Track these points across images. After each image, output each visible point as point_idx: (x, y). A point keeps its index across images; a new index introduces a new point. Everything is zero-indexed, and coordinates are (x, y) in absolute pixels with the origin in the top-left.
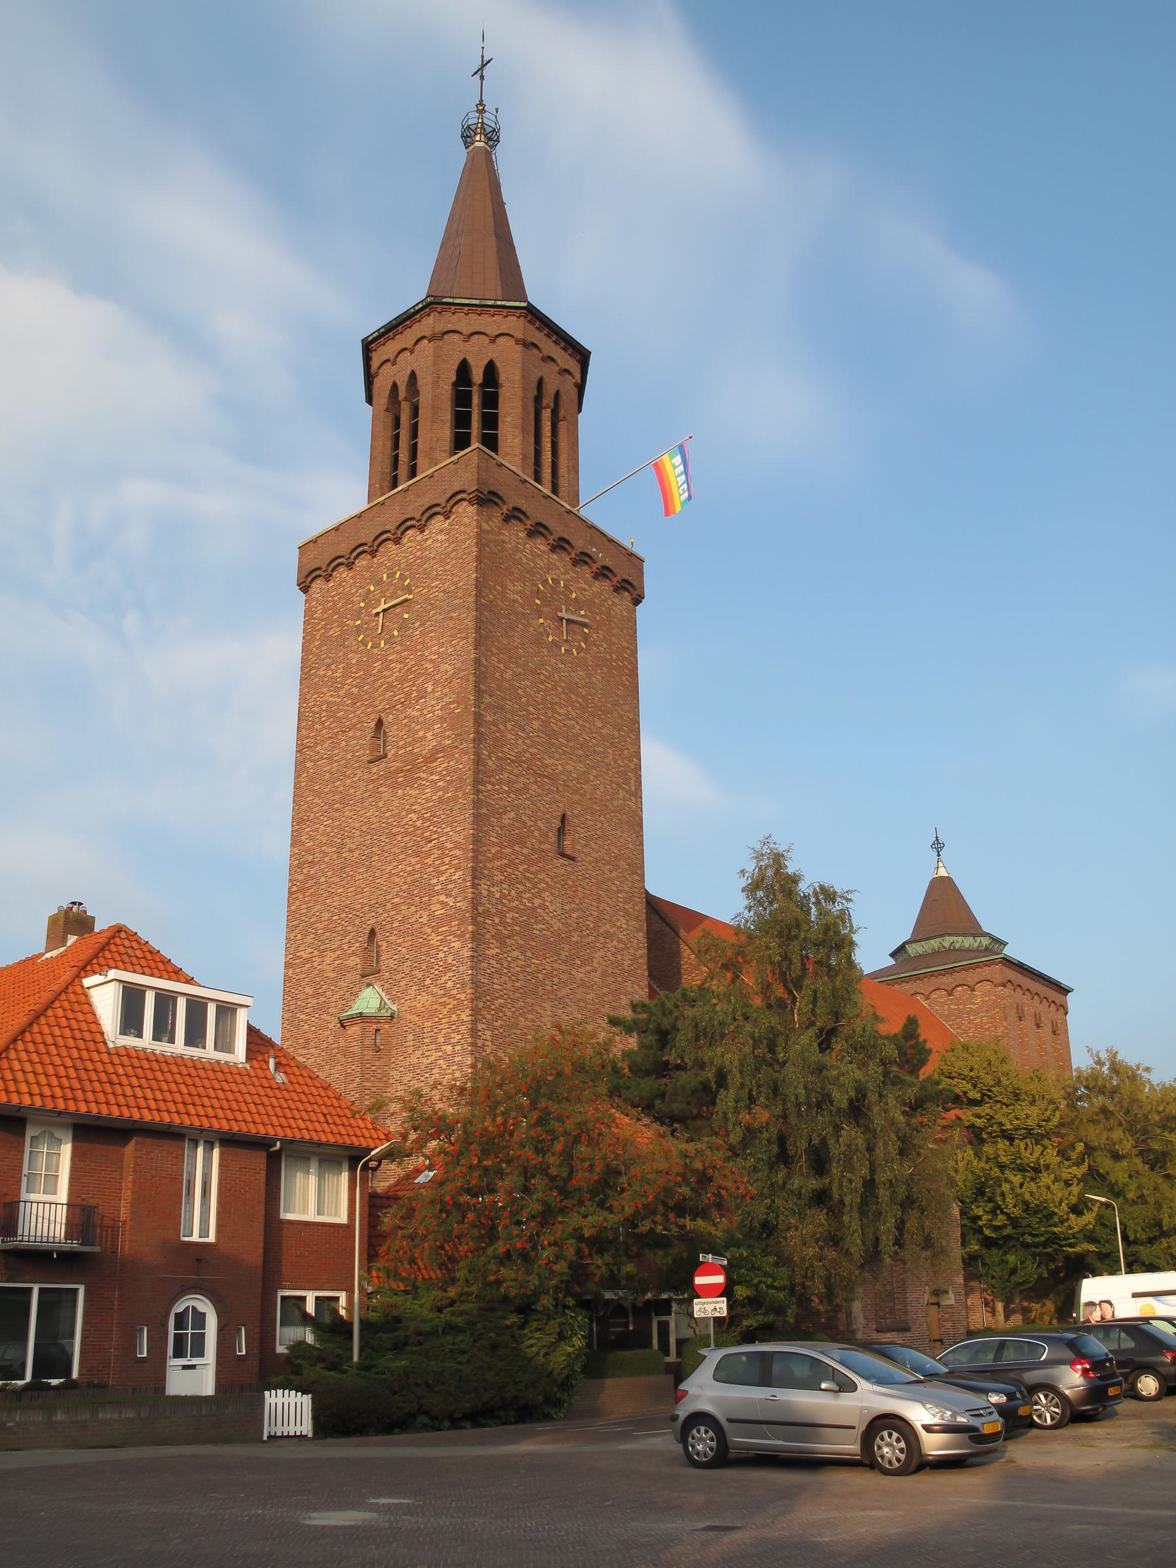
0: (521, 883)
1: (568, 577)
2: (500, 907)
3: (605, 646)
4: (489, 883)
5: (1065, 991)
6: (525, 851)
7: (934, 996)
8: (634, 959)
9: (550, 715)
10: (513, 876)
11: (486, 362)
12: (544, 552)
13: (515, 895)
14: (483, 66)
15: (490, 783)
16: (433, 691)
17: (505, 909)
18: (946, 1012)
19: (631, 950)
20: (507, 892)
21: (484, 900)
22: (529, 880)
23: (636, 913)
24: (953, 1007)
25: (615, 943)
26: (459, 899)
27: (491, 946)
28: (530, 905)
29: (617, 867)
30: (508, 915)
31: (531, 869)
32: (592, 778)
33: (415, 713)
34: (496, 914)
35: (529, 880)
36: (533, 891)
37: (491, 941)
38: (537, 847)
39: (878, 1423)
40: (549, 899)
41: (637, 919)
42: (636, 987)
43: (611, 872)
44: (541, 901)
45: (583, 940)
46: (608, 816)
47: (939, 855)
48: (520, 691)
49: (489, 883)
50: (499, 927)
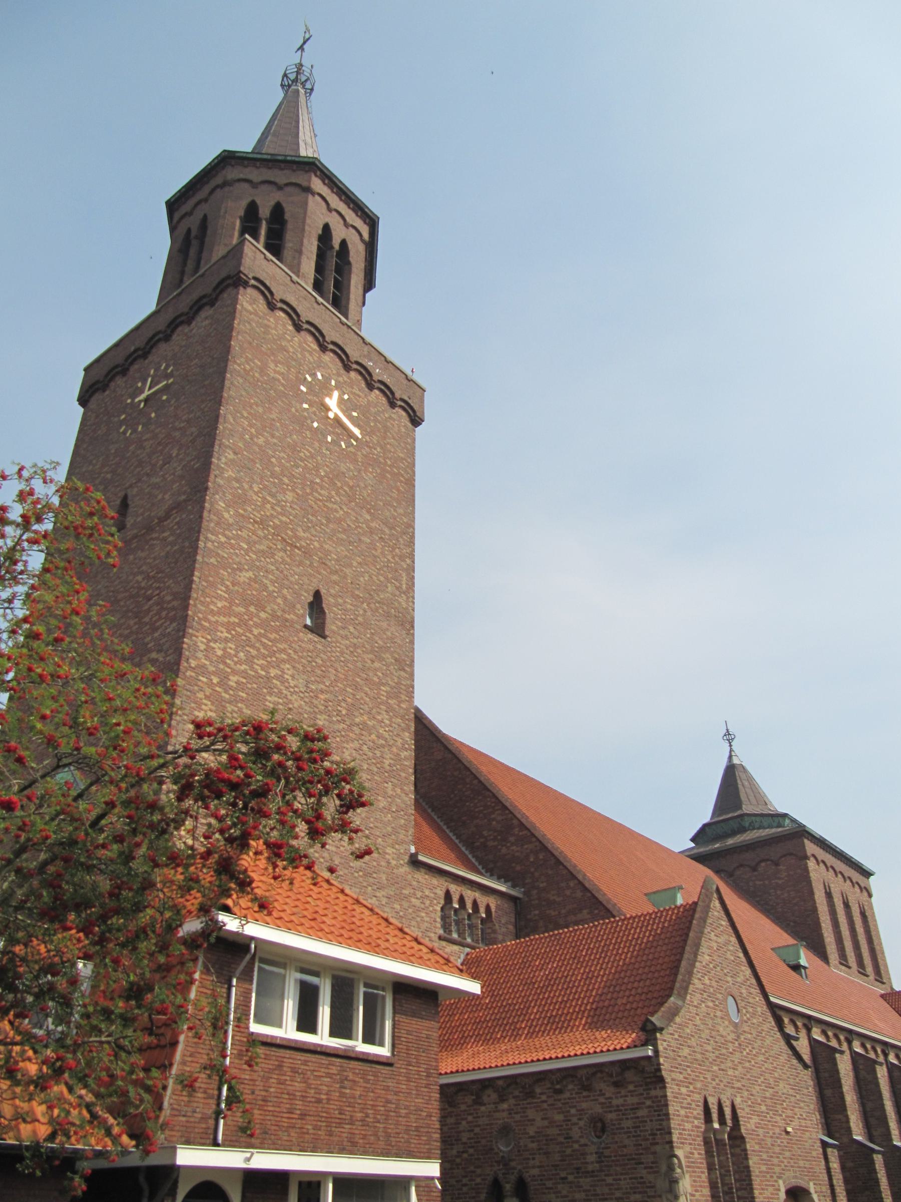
0: (253, 647)
1: (341, 379)
2: (221, 666)
3: (379, 450)
4: (209, 637)
5: (867, 874)
6: (263, 615)
7: (738, 873)
8: (397, 758)
9: (308, 491)
10: (243, 638)
11: (272, 203)
12: (315, 350)
13: (244, 658)
14: (305, 43)
15: (224, 535)
16: (178, 455)
17: (229, 670)
18: (752, 889)
19: (394, 749)
20: (232, 652)
21: (200, 655)
22: (265, 646)
23: (402, 711)
24: (758, 883)
25: (373, 737)
26: (170, 651)
27: (203, 707)
28: (263, 673)
29: (381, 659)
30: (231, 677)
31: (269, 635)
32: (355, 564)
33: (158, 480)
34: (214, 673)
35: (265, 646)
36: (269, 659)
37: (205, 701)
38: (279, 614)
39: (232, 173)
40: (290, 673)
41: (402, 717)
42: (399, 791)
43: (373, 661)
44: (280, 673)
45: (331, 725)
46: (372, 606)
47: (731, 746)
48: (273, 460)
49: (209, 637)
50: (217, 689)
